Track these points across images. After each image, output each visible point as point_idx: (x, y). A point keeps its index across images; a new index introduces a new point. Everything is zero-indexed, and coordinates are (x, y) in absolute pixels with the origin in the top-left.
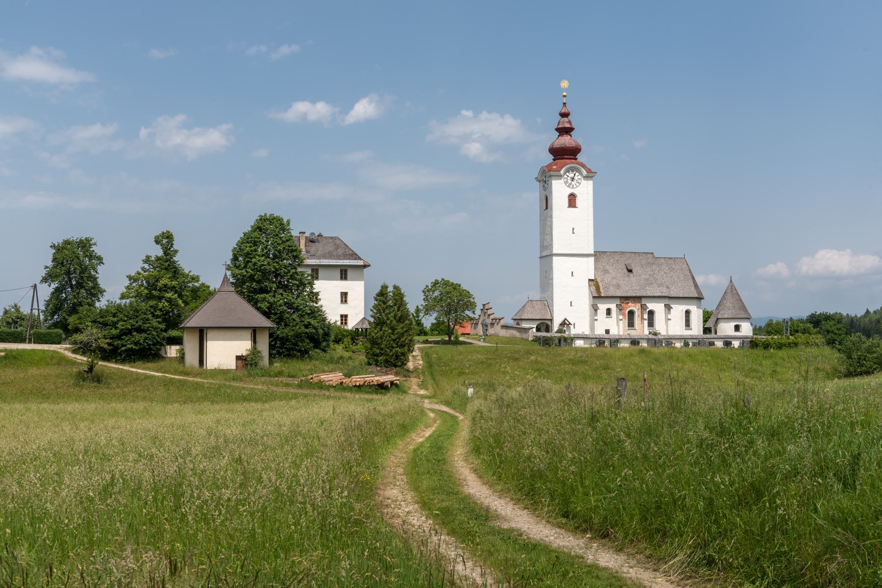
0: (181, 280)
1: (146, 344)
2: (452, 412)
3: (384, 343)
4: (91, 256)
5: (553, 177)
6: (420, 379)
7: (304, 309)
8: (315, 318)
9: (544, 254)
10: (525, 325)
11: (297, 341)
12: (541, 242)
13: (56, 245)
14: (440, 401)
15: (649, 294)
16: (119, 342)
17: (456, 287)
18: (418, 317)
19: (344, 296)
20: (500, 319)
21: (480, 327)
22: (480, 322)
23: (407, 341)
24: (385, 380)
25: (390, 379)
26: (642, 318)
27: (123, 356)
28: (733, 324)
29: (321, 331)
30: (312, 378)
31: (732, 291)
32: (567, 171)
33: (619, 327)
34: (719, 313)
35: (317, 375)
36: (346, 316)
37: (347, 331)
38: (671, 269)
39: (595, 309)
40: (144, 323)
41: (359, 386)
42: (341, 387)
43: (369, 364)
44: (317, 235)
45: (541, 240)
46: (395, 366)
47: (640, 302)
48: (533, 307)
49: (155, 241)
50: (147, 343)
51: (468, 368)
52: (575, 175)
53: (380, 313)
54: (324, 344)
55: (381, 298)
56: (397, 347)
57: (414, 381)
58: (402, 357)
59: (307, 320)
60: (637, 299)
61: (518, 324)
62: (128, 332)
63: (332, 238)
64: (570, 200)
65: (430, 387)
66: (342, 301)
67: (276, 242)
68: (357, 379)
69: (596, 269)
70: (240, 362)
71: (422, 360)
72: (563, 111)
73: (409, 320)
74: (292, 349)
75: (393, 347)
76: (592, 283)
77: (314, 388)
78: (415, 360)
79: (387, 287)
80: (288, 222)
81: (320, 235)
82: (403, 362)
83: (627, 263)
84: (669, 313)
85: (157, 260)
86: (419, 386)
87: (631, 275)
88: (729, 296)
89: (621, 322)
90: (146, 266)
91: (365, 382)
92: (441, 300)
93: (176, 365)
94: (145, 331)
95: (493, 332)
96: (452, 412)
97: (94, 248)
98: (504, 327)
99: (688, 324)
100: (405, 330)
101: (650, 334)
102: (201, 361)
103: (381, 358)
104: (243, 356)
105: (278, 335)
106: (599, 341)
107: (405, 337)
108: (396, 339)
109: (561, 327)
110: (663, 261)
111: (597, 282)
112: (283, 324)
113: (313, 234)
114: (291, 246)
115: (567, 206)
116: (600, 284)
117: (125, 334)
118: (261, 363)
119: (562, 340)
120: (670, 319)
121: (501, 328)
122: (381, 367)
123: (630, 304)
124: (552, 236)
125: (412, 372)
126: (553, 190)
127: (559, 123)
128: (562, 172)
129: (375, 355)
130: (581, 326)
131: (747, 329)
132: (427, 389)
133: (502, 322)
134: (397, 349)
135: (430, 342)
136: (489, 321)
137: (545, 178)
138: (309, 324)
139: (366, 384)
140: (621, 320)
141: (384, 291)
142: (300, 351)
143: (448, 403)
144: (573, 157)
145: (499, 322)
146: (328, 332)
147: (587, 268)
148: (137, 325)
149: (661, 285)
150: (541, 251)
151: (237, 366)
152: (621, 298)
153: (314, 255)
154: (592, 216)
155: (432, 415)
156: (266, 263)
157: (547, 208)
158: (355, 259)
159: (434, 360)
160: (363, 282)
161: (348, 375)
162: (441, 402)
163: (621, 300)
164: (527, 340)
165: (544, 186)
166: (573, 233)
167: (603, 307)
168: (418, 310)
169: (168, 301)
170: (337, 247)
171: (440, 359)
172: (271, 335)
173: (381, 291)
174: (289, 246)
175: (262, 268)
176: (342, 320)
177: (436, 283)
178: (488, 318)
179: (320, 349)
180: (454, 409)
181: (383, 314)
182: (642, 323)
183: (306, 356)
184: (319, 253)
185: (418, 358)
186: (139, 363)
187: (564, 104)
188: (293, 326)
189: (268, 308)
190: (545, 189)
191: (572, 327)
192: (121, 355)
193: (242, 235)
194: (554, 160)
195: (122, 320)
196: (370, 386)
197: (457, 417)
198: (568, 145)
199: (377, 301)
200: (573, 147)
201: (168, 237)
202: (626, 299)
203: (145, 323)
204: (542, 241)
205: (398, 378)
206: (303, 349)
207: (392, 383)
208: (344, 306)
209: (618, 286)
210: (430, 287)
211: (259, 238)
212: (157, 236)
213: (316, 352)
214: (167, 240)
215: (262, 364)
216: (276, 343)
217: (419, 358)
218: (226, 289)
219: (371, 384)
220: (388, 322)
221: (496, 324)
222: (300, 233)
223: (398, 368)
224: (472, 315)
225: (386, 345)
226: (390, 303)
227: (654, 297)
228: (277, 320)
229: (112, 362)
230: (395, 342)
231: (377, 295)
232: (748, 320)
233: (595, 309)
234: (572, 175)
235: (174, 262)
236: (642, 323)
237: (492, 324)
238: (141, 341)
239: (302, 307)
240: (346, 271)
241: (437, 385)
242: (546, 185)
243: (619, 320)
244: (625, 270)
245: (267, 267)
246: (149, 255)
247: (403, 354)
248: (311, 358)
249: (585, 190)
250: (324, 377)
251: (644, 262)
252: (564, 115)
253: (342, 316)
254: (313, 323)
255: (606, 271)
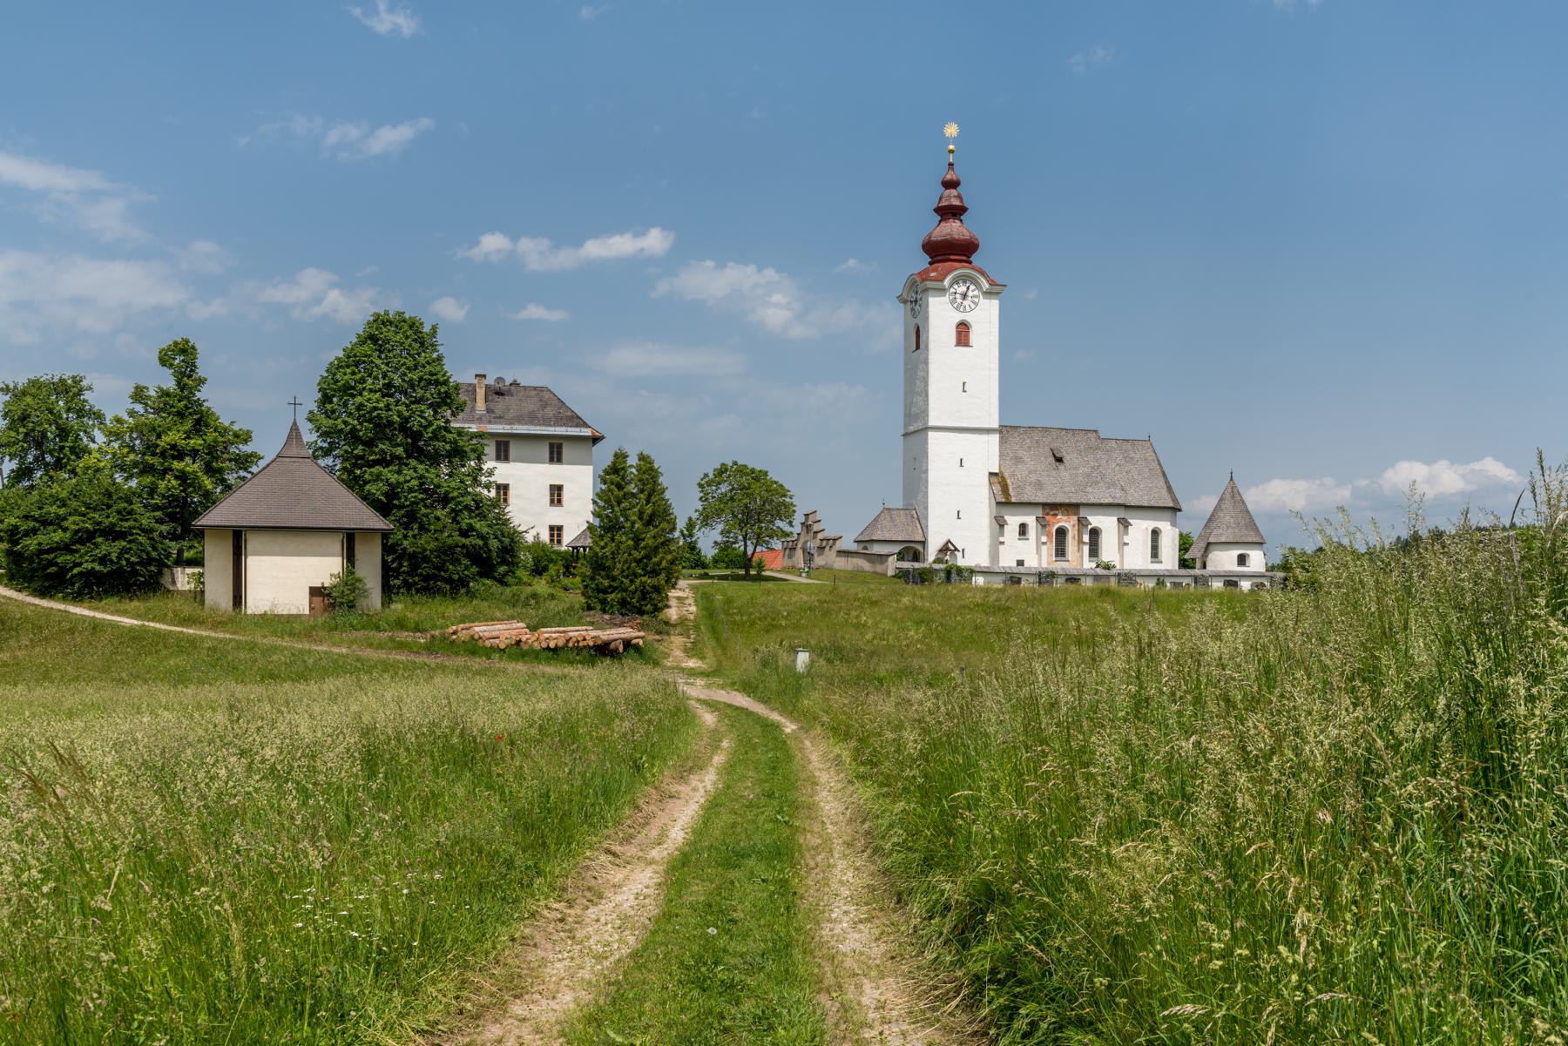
0: (211, 436)
1: (124, 563)
2: (759, 709)
3: (619, 566)
4: (81, 410)
5: (930, 292)
6: (689, 638)
7: (461, 499)
8: (483, 517)
9: (911, 429)
10: (877, 549)
11: (445, 561)
12: (905, 409)
13: (11, 386)
14: (730, 681)
15: (1093, 500)
16: (68, 557)
17: (759, 476)
18: (691, 536)
19: (556, 494)
20: (835, 540)
21: (799, 553)
22: (799, 546)
23: (664, 563)
24: (612, 637)
25: (623, 636)
26: (1080, 542)
27: (77, 585)
28: (1235, 553)
29: (494, 544)
30: (455, 633)
31: (1233, 497)
32: (956, 281)
33: (1040, 556)
34: (1210, 534)
35: (467, 625)
36: (560, 528)
37: (558, 553)
38: (1128, 459)
39: (1000, 524)
40: (121, 520)
41: (556, 650)
42: (517, 650)
43: (589, 608)
44: (508, 383)
45: (906, 406)
46: (641, 612)
47: (1077, 514)
48: (892, 520)
49: (160, 359)
50: (127, 560)
51: (786, 618)
52: (968, 288)
53: (612, 507)
54: (502, 569)
55: (613, 477)
56: (644, 576)
57: (677, 642)
58: (654, 595)
59: (466, 520)
60: (1072, 508)
61: (865, 548)
62: (85, 537)
63: (535, 388)
64: (959, 333)
65: (710, 654)
66: (552, 501)
67: (404, 364)
68: (552, 635)
69: (1001, 455)
70: (318, 600)
71: (696, 605)
72: (949, 177)
73: (668, 523)
74: (434, 577)
75: (636, 575)
76: (994, 479)
77: (457, 654)
78: (682, 600)
79: (625, 456)
80: (434, 329)
81: (515, 384)
82: (656, 605)
83: (1054, 446)
84: (1127, 533)
85: (160, 397)
86: (686, 650)
87: (1061, 467)
88: (1227, 504)
89: (1044, 548)
90: (139, 408)
91: (568, 641)
92: (732, 499)
93: (188, 609)
94: (120, 535)
95: (823, 563)
96: (759, 709)
97: (87, 395)
98: (841, 553)
99: (1155, 554)
100: (660, 541)
101: (1098, 566)
102: (238, 598)
103: (613, 596)
104: (325, 588)
105: (405, 548)
106: (1011, 577)
107: (661, 555)
108: (643, 558)
109: (941, 556)
110: (1114, 444)
111: (1003, 478)
112: (416, 526)
113: (500, 379)
114: (436, 374)
115: (954, 342)
116: (1009, 481)
117: (81, 542)
118: (362, 603)
119: (954, 571)
120: (1127, 544)
121: (837, 556)
122: (612, 613)
123: (1059, 517)
124: (927, 395)
125: (674, 626)
126: (930, 314)
127: (941, 199)
128: (946, 282)
129: (599, 590)
130: (974, 554)
131: (1257, 561)
132: (703, 658)
133: (840, 545)
134: (644, 579)
135: (713, 577)
136: (813, 545)
137: (914, 298)
138: (471, 528)
139: (570, 645)
140: (1044, 543)
141: (620, 464)
142: (449, 581)
143: (748, 688)
144: (965, 258)
145: (834, 544)
146: (512, 548)
147: (986, 454)
148: (107, 522)
149: (1112, 485)
150: (905, 425)
151: (311, 609)
152: (1044, 505)
153: (500, 417)
154: (997, 361)
155: (709, 718)
156: (381, 405)
157: (918, 347)
158: (577, 426)
159: (717, 603)
160: (591, 468)
161: (533, 628)
162: (733, 684)
163: (1044, 509)
164: (884, 575)
165: (913, 309)
166: (964, 391)
167: (1013, 521)
168: (691, 525)
169: (177, 478)
170: (545, 404)
171: (729, 601)
172: (387, 549)
173: (614, 463)
174: (431, 374)
175: (375, 414)
176: (552, 535)
177: (722, 471)
178: (815, 537)
179: (495, 579)
180: (765, 701)
181: (617, 509)
182: (1080, 550)
183: (463, 591)
184: (512, 413)
185: (687, 602)
186: (111, 601)
187: (951, 165)
188: (436, 531)
189: (386, 495)
190: (914, 313)
191: (959, 555)
192: (73, 585)
193: (341, 354)
194: (931, 264)
195: (76, 512)
196: (578, 650)
197: (776, 727)
198: (956, 237)
199: (605, 484)
200: (965, 240)
201: (183, 351)
202: (1053, 507)
203: (127, 520)
204: (908, 406)
205: (642, 634)
206: (456, 577)
207: (627, 644)
208: (556, 509)
209: (1039, 485)
210: (711, 476)
211: (370, 356)
212: (163, 349)
213: (484, 585)
214: (182, 358)
215: (364, 604)
216: (401, 565)
217: (691, 601)
218: (294, 451)
219: (581, 644)
220: (628, 525)
221: (827, 548)
222: (476, 376)
223: (645, 617)
224: (787, 528)
225: (623, 571)
226: (632, 488)
227: (1101, 505)
228: (405, 520)
229: (58, 600)
230: (641, 565)
231: (607, 472)
232: (1259, 546)
233: (1000, 524)
234: (962, 289)
235: (199, 403)
236: (1080, 550)
237: (822, 549)
238: (114, 556)
239: (455, 494)
240: (560, 447)
241: (724, 649)
242: (917, 308)
243: (1039, 544)
244: (1052, 459)
245: (384, 414)
246: (142, 384)
247: (657, 589)
248: (472, 595)
249: (986, 315)
250: (480, 629)
251: (1082, 446)
252: (950, 184)
253: (552, 528)
254: (478, 526)
255: (1018, 460)
